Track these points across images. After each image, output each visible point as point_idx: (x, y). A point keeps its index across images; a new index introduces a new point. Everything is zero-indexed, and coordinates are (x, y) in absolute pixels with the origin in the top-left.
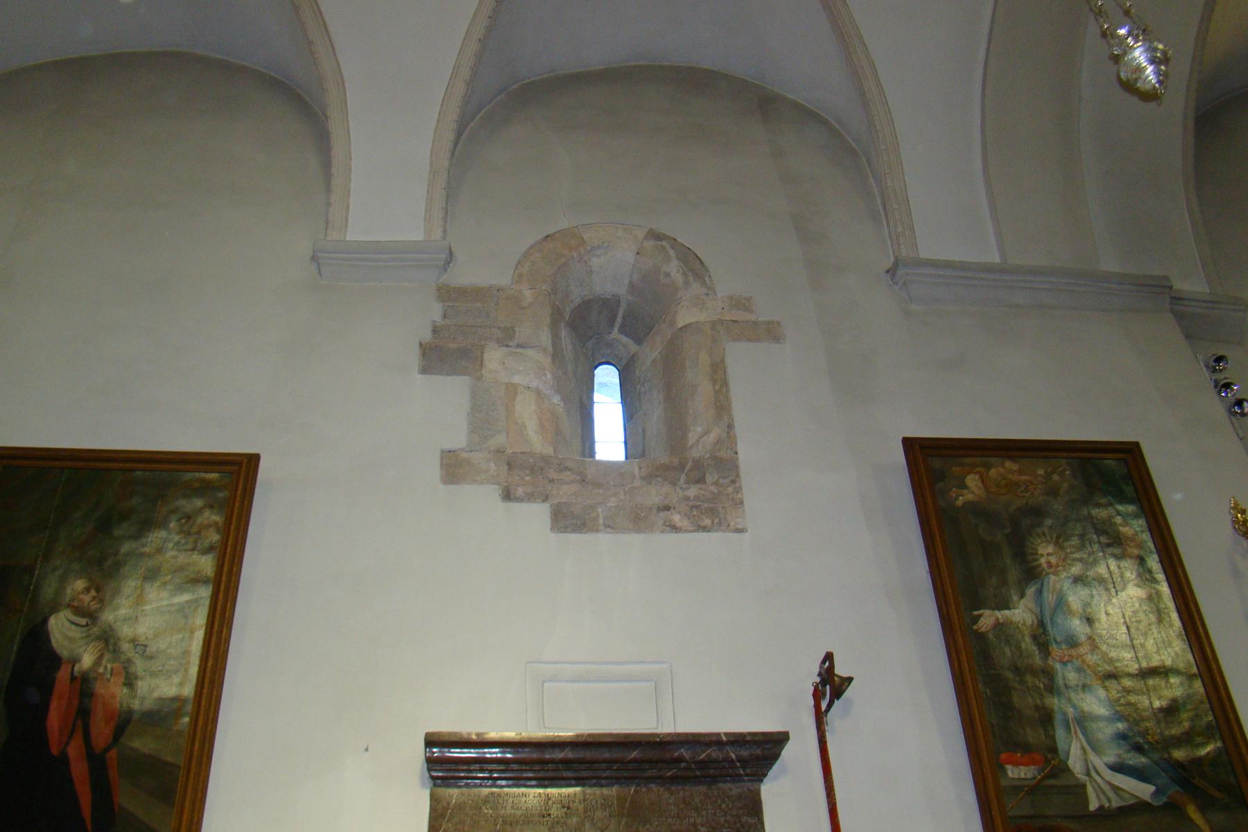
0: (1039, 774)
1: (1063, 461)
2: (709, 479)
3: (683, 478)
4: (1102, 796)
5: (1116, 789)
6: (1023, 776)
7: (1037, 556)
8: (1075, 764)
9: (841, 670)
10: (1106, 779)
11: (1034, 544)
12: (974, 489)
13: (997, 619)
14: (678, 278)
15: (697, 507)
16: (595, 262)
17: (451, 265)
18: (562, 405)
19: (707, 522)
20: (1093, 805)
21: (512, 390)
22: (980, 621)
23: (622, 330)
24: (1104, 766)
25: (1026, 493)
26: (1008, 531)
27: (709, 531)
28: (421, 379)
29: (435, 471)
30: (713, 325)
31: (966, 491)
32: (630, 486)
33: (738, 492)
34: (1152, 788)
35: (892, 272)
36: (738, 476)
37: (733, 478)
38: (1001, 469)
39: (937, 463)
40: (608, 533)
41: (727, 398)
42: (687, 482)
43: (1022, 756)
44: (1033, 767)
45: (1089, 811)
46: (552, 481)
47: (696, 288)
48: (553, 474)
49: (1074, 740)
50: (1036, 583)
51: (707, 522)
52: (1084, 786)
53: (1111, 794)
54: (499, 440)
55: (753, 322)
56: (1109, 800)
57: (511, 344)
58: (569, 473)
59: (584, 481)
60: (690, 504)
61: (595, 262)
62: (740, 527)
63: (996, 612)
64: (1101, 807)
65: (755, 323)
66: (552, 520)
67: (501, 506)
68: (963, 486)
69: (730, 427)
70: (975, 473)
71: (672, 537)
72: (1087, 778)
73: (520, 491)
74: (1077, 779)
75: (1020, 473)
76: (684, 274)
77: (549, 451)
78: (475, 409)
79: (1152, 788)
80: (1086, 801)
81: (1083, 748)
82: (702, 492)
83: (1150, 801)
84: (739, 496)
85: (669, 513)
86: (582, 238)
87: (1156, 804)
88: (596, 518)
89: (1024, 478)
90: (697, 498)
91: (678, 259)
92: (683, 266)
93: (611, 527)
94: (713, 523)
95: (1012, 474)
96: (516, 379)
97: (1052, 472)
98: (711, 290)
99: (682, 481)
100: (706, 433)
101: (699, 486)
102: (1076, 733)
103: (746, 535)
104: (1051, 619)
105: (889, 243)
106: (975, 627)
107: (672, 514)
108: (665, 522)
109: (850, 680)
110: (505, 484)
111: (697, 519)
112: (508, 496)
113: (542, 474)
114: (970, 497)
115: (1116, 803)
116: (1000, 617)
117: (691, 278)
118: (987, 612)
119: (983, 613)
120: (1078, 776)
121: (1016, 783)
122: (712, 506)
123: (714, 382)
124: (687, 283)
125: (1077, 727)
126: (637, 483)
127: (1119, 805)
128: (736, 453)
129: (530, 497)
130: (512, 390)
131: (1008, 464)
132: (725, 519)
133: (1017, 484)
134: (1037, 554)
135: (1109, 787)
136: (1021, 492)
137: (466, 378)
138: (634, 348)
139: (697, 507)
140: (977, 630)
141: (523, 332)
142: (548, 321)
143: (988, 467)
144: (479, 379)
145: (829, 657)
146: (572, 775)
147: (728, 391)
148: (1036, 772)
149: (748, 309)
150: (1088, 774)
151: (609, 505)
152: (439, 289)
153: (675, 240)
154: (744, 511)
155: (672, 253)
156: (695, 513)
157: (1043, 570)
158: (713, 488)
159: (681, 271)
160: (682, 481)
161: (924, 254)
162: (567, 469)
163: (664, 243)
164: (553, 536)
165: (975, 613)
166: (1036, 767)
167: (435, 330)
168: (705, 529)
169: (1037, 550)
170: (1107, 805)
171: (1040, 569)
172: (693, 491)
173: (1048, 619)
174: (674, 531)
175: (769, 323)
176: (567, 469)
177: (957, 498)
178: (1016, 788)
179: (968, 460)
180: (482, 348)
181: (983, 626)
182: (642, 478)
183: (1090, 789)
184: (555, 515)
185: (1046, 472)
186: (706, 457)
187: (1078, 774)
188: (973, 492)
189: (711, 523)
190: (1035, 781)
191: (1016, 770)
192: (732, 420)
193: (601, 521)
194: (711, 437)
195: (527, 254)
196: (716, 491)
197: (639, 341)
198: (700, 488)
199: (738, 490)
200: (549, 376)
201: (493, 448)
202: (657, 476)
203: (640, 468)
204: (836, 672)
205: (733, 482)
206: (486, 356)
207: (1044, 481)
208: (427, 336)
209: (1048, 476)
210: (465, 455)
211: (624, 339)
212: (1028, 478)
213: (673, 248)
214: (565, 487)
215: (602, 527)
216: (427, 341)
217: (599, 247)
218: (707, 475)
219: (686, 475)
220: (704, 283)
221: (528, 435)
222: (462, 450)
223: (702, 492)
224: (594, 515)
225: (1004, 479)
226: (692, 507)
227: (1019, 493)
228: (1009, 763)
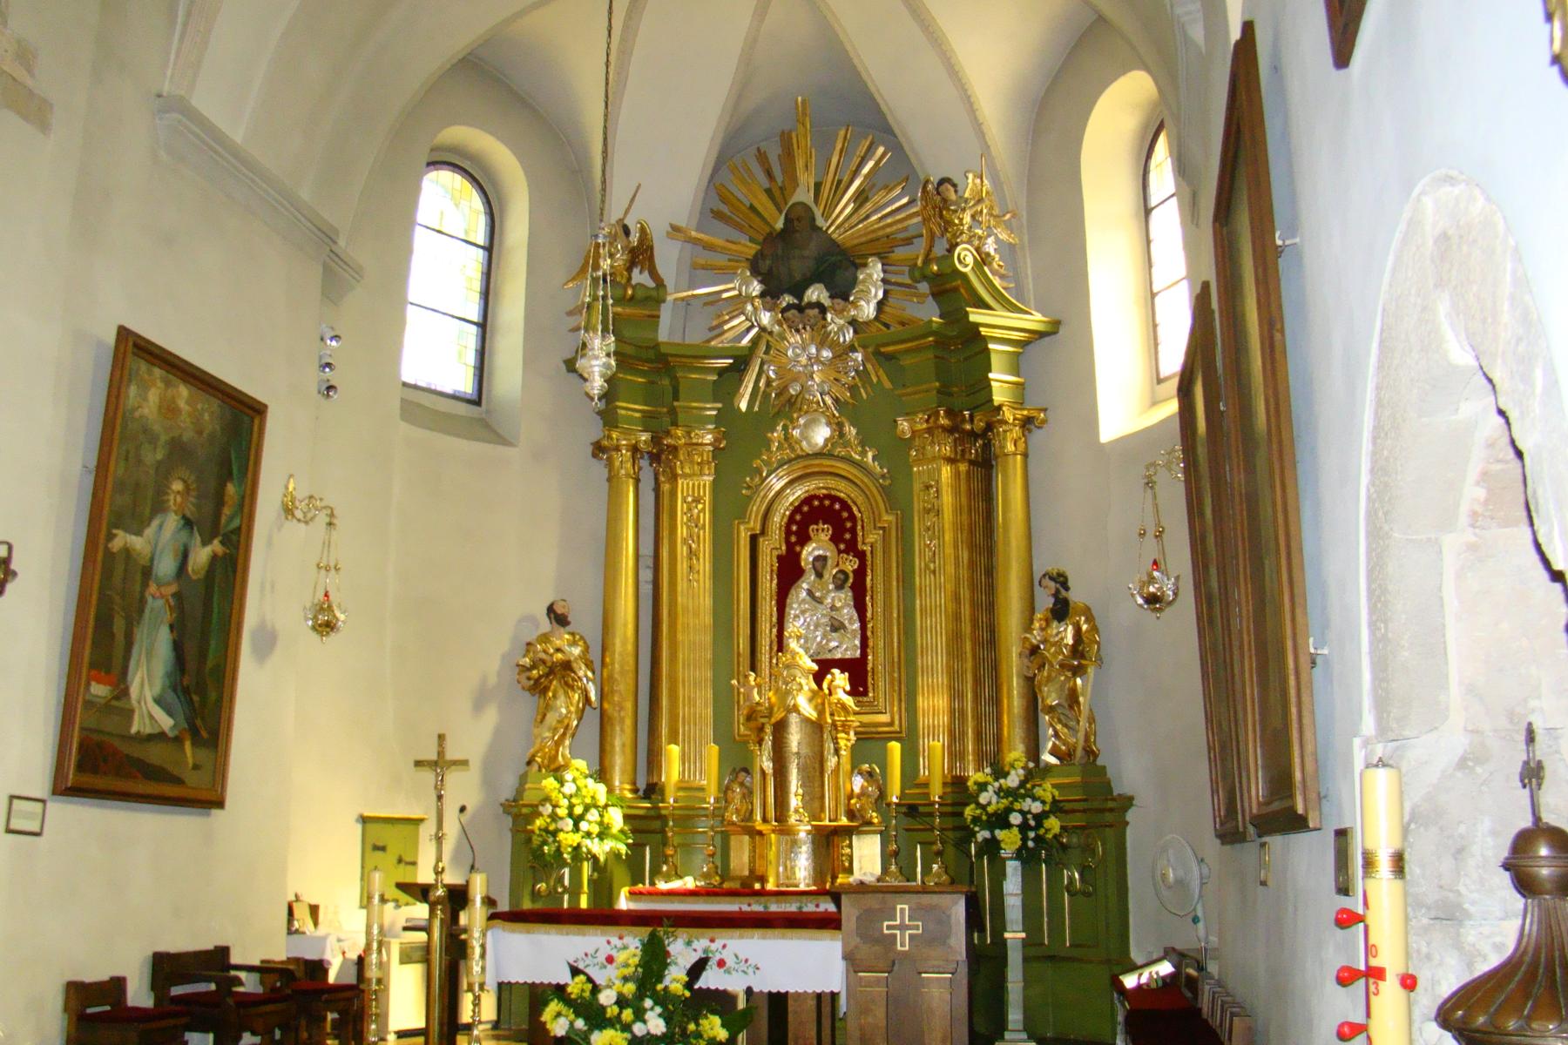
5: (151, 717)
20: (134, 730)
53: (147, 721)
64: (139, 732)
115: (148, 730)
150: (139, 703)
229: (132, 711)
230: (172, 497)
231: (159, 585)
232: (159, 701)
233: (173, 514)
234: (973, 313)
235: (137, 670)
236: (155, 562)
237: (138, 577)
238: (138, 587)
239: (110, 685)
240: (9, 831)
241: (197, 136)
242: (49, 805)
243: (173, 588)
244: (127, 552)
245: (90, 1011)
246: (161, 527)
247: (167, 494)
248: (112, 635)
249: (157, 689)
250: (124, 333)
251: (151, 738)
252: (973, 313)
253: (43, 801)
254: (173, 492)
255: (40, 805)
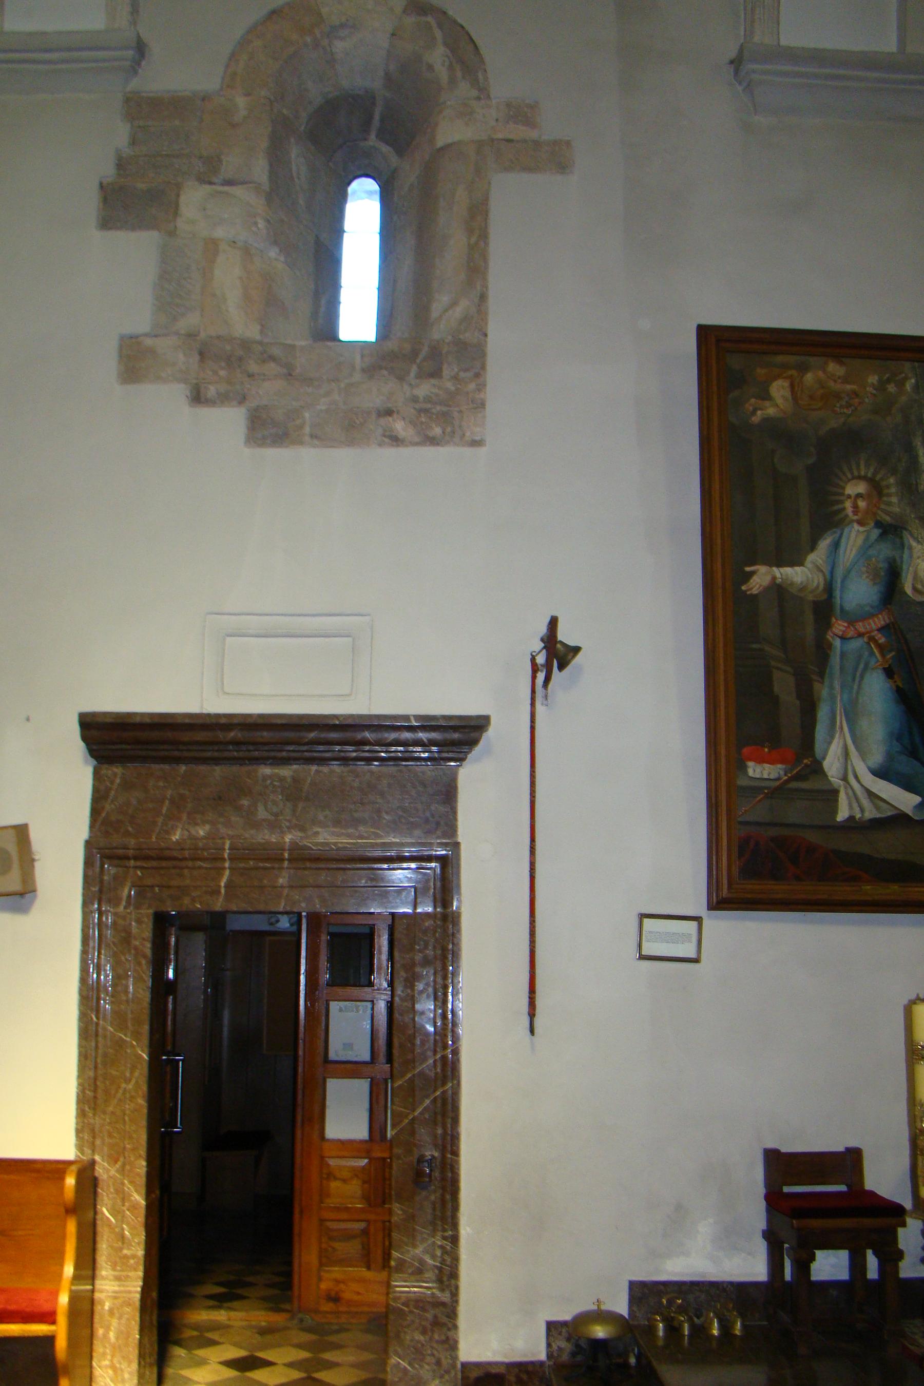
0: (785, 775)
1: (908, 365)
2: (446, 372)
3: (414, 370)
4: (855, 805)
5: (871, 795)
6: (766, 776)
7: (842, 498)
8: (832, 765)
9: (565, 635)
10: (864, 784)
11: (841, 479)
12: (779, 401)
13: (774, 578)
14: (443, 74)
15: (426, 411)
16: (339, 46)
17: (143, 63)
18: (282, 258)
19: (437, 431)
20: (842, 815)
21: (212, 247)
22: (751, 581)
23: (381, 135)
24: (867, 770)
25: (847, 408)
26: (811, 461)
27: (438, 444)
28: (98, 235)
29: (111, 364)
30: (480, 144)
31: (767, 403)
32: (346, 381)
33: (479, 390)
34: (917, 799)
35: (736, 63)
36: (483, 367)
37: (477, 371)
38: (820, 373)
39: (735, 362)
40: (314, 446)
41: (484, 257)
42: (419, 376)
43: (770, 752)
44: (779, 766)
45: (836, 820)
46: (251, 376)
47: (464, 89)
48: (253, 367)
49: (837, 735)
50: (835, 532)
51: (437, 431)
52: (836, 792)
53: (865, 802)
54: (191, 321)
55: (534, 141)
56: (862, 810)
57: (215, 180)
58: (272, 365)
59: (290, 375)
60: (417, 406)
61: (339, 46)
62: (477, 438)
63: (774, 569)
64: (851, 818)
65: (537, 144)
66: (248, 428)
67: (186, 410)
68: (765, 396)
69: (483, 297)
70: (785, 378)
71: (390, 452)
72: (841, 783)
73: (212, 391)
74: (830, 783)
75: (846, 380)
76: (451, 68)
77: (253, 332)
78: (164, 276)
79: (917, 799)
80: (835, 812)
81: (846, 748)
82: (436, 390)
83: (910, 814)
84: (482, 396)
85: (390, 419)
86: (320, 15)
87: (916, 818)
88: (301, 427)
89: (849, 387)
90: (428, 399)
91: (446, 44)
92: (450, 55)
93: (319, 438)
94: (444, 432)
95: (835, 381)
96: (220, 233)
97: (889, 381)
98: (483, 92)
99: (412, 374)
100: (454, 304)
101: (433, 381)
102: (841, 728)
103: (482, 451)
104: (843, 581)
105: (743, 17)
106: (744, 588)
107: (394, 421)
108: (385, 431)
109: (576, 650)
110: (195, 381)
111: (424, 427)
112: (198, 398)
113: (240, 367)
114: (771, 411)
115: (870, 813)
116: (778, 575)
117: (459, 74)
118: (762, 569)
119: (758, 570)
120: (832, 779)
121: (756, 784)
122: (445, 409)
123: (470, 231)
124: (452, 81)
125: (844, 718)
126: (357, 377)
127: (872, 816)
128: (486, 335)
129: (223, 399)
130: (212, 247)
131: (832, 367)
132: (460, 427)
133: (837, 396)
134: (843, 494)
135: (866, 795)
136: (841, 407)
137: (155, 234)
138: (394, 160)
139: (426, 411)
140: (746, 591)
141: (231, 163)
142: (264, 144)
143: (803, 368)
144: (172, 233)
145: (553, 623)
146: (259, 733)
147: (487, 244)
148: (782, 773)
149: (530, 123)
150: (845, 778)
151: (319, 407)
152: (127, 100)
153: (445, 13)
154: (484, 417)
155: (438, 34)
156: (423, 420)
157: (847, 516)
158: (450, 385)
159: (447, 64)
160: (412, 374)
161: (789, 38)
162: (272, 358)
163: (429, 19)
164: (247, 451)
165: (748, 569)
166: (784, 766)
167: (121, 164)
168: (433, 441)
169: (844, 488)
170: (858, 816)
171: (841, 516)
172: (424, 389)
173: (839, 581)
174: (395, 443)
175: (555, 143)
176: (272, 358)
177: (754, 413)
178: (755, 789)
179: (780, 359)
180: (179, 186)
181: (754, 587)
182: (363, 370)
183: (842, 797)
184: (252, 422)
185: (880, 381)
186: (447, 341)
187: (833, 777)
188: (777, 405)
189: (441, 432)
190: (777, 783)
191: (758, 768)
192: (487, 287)
193: (307, 430)
194: (458, 312)
195: (244, 42)
196: (453, 388)
197: (400, 151)
198: (434, 385)
199: (481, 387)
200: (261, 224)
201: (183, 332)
202: (381, 368)
203: (362, 356)
204: (560, 637)
205: (477, 375)
206: (183, 199)
207: (874, 392)
208: (108, 171)
209: (881, 387)
210: (149, 342)
211: (385, 149)
212: (854, 387)
213: (440, 26)
214: (266, 384)
215: (307, 438)
216: (110, 180)
217: (342, 26)
218: (445, 366)
219: (419, 367)
220: (475, 83)
221: (227, 311)
222: (146, 335)
223: (436, 390)
224: (298, 422)
225: (823, 387)
226: (420, 411)
227: (838, 409)
228: (750, 760)
229: (834, 793)
230: (848, 504)
231: (851, 623)
232: (881, 773)
233: (856, 527)
234: (778, 668)
235: (832, 737)
236: (837, 594)
237: (809, 617)
238: (810, 631)
239: (782, 763)
240: (642, 957)
241: (786, 74)
242: (706, 923)
243: (881, 620)
244: (779, 590)
245: (786, 1189)
246: (836, 545)
247: (842, 502)
248: (775, 700)
249: (877, 757)
250: (705, 333)
251: (877, 824)
252: (778, 668)
253: (698, 919)
254: (849, 497)
255: (694, 924)
